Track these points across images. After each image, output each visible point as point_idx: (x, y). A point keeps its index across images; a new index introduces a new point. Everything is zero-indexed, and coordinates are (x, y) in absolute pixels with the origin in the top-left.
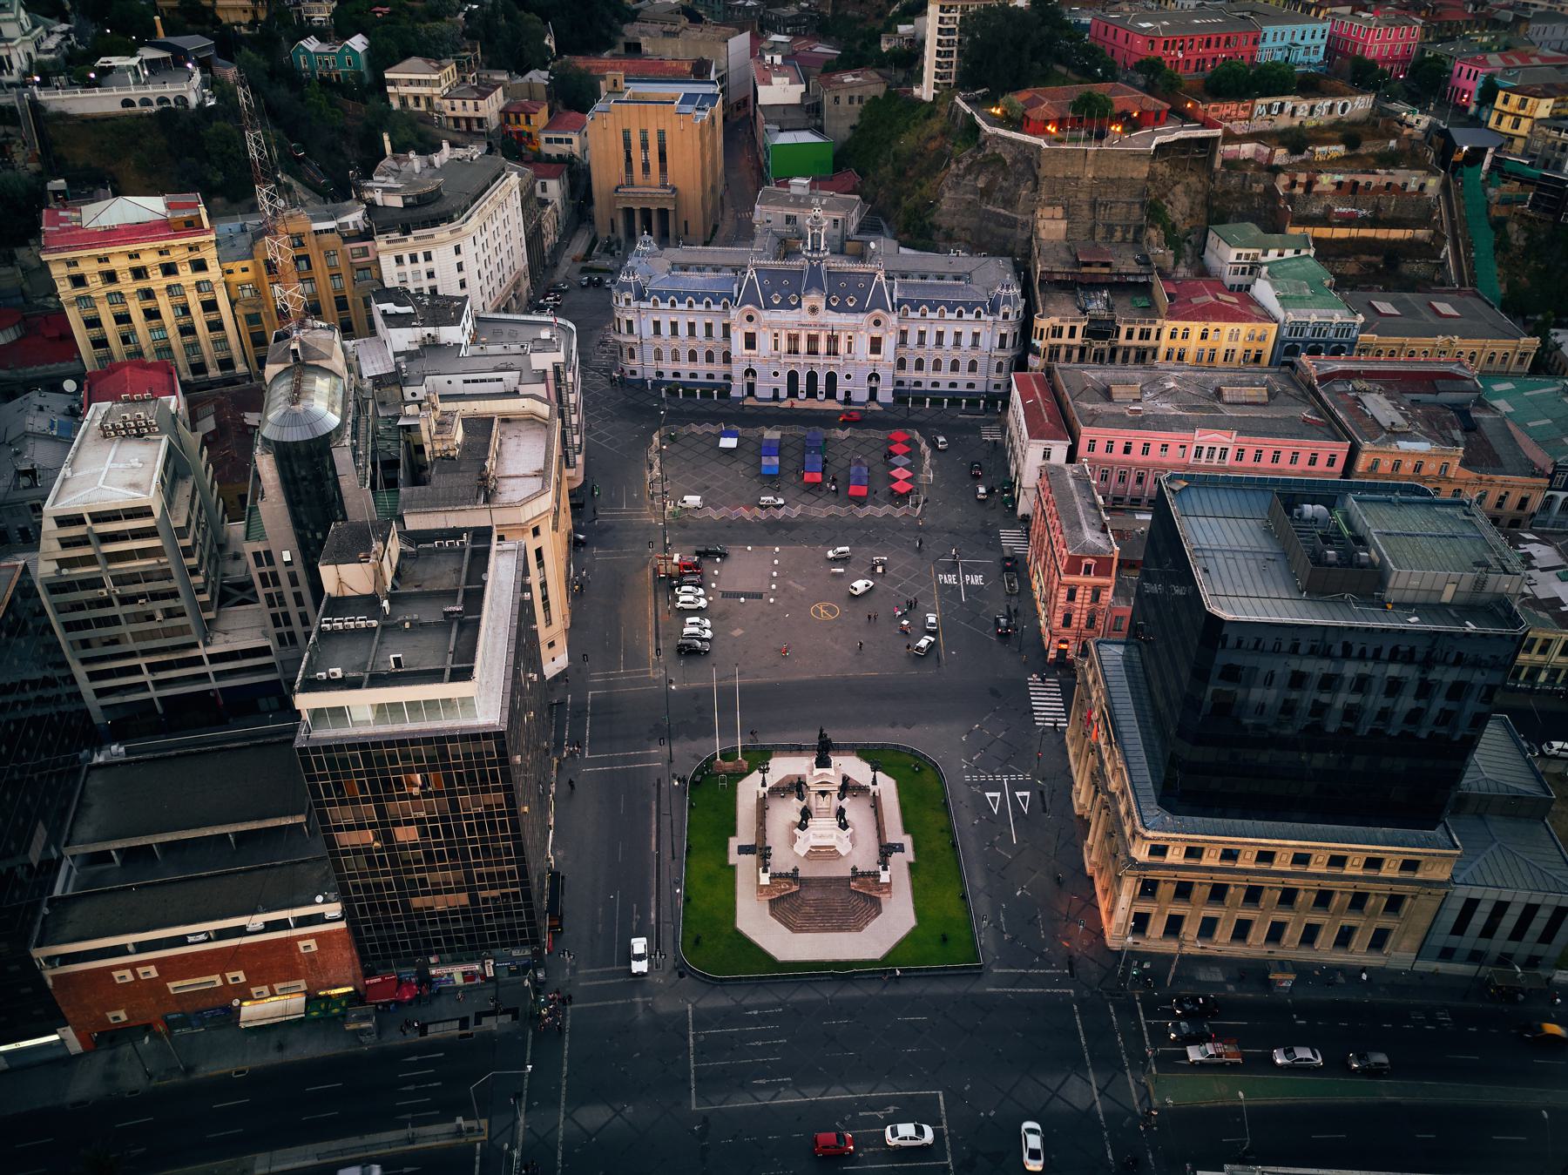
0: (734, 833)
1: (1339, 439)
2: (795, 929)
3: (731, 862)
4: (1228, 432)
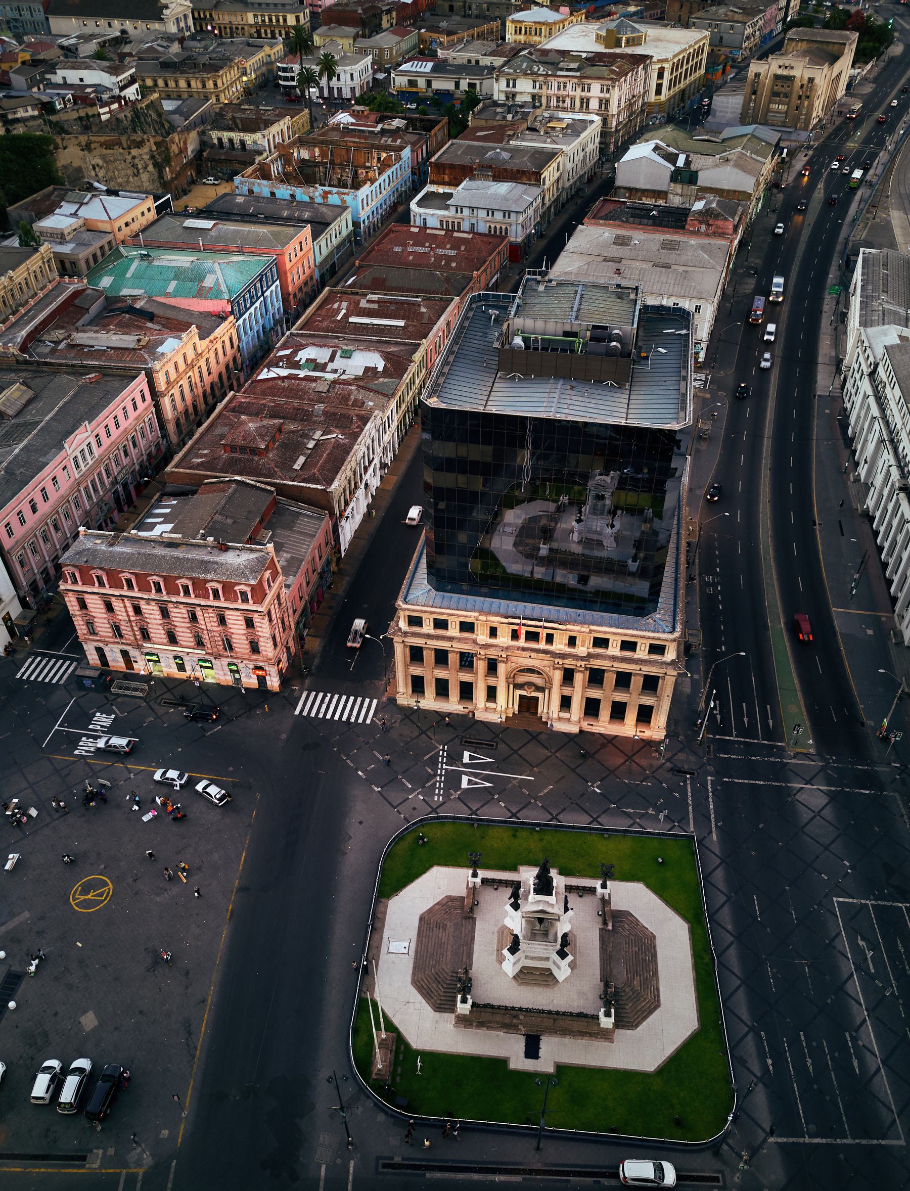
0: (502, 1063)
1: (135, 377)
2: (655, 1004)
3: (551, 1070)
4: (81, 429)
